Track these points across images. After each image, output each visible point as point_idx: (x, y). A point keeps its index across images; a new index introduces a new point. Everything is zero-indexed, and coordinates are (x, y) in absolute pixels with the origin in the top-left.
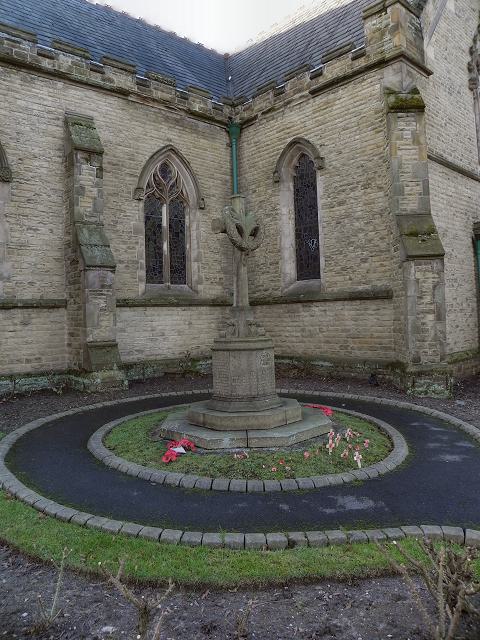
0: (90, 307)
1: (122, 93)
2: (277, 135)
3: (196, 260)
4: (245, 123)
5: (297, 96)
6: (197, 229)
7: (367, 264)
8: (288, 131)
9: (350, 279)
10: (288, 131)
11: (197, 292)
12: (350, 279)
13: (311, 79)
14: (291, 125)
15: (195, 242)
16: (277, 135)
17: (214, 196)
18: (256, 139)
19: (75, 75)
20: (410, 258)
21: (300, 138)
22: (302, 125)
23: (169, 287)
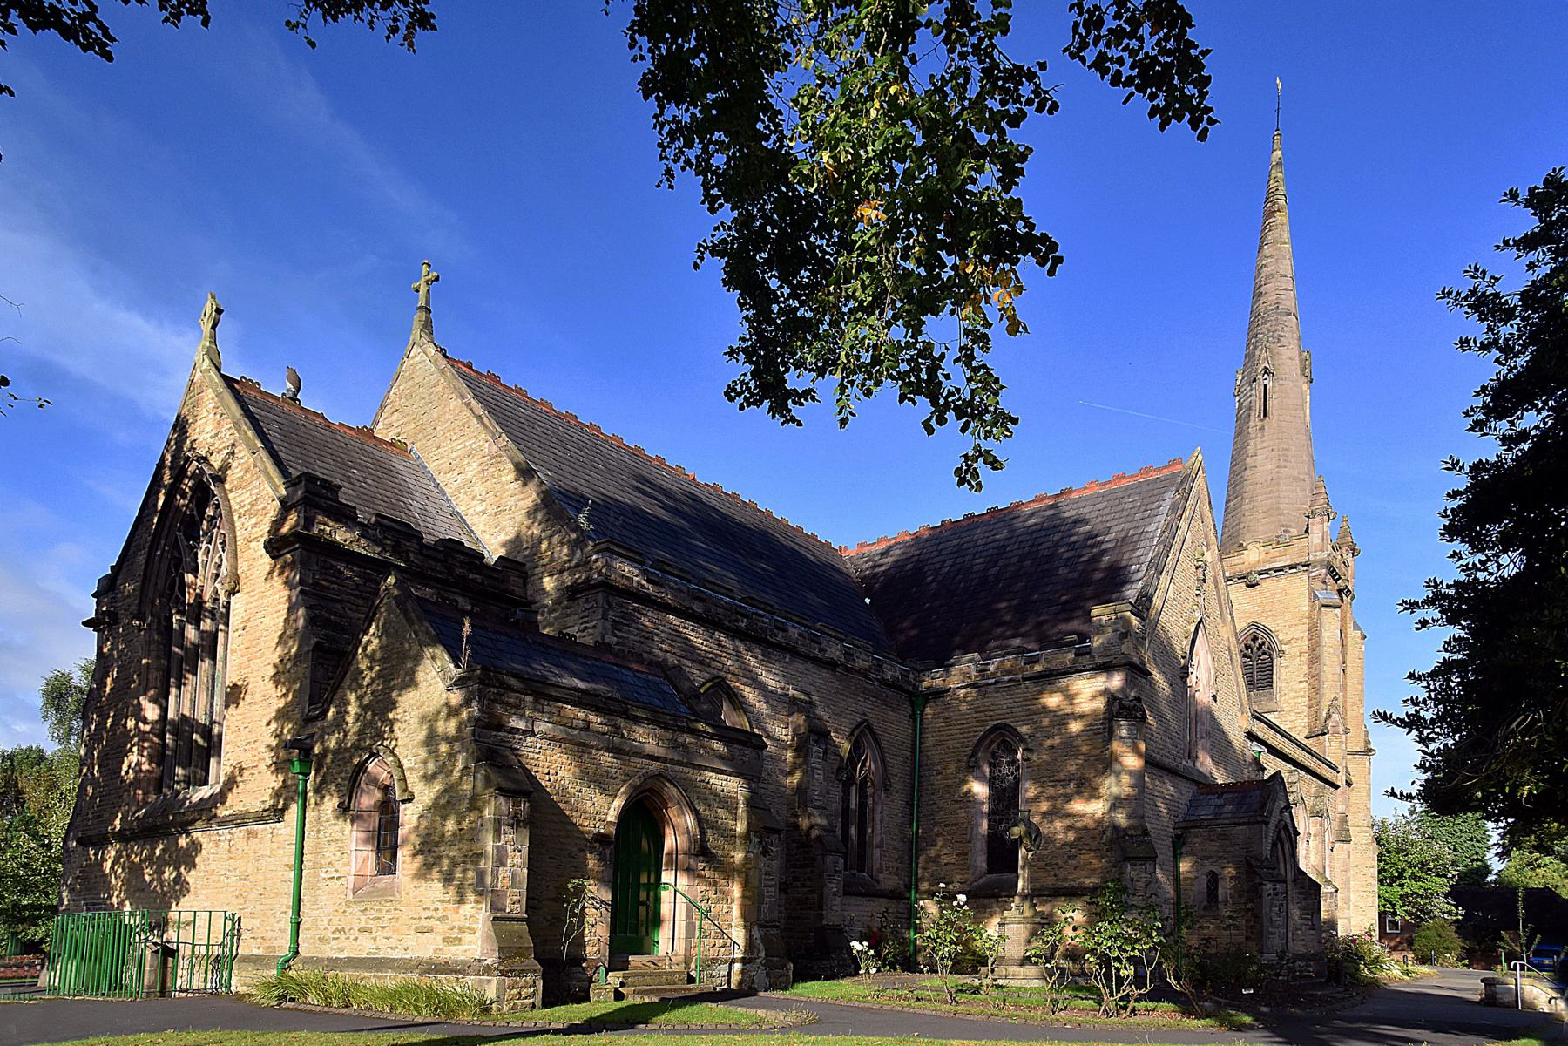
0: (826, 891)
1: (831, 665)
2: (975, 715)
3: (878, 847)
4: (931, 694)
5: (1006, 678)
6: (882, 812)
7: (1074, 862)
8: (991, 713)
9: (1055, 875)
10: (991, 713)
11: (878, 882)
12: (1055, 875)
13: (1025, 664)
14: (994, 707)
15: (879, 827)
16: (975, 715)
17: (896, 776)
18: (946, 715)
19: (802, 649)
20: (1127, 859)
21: (1005, 725)
22: (1008, 711)
23: (854, 875)
